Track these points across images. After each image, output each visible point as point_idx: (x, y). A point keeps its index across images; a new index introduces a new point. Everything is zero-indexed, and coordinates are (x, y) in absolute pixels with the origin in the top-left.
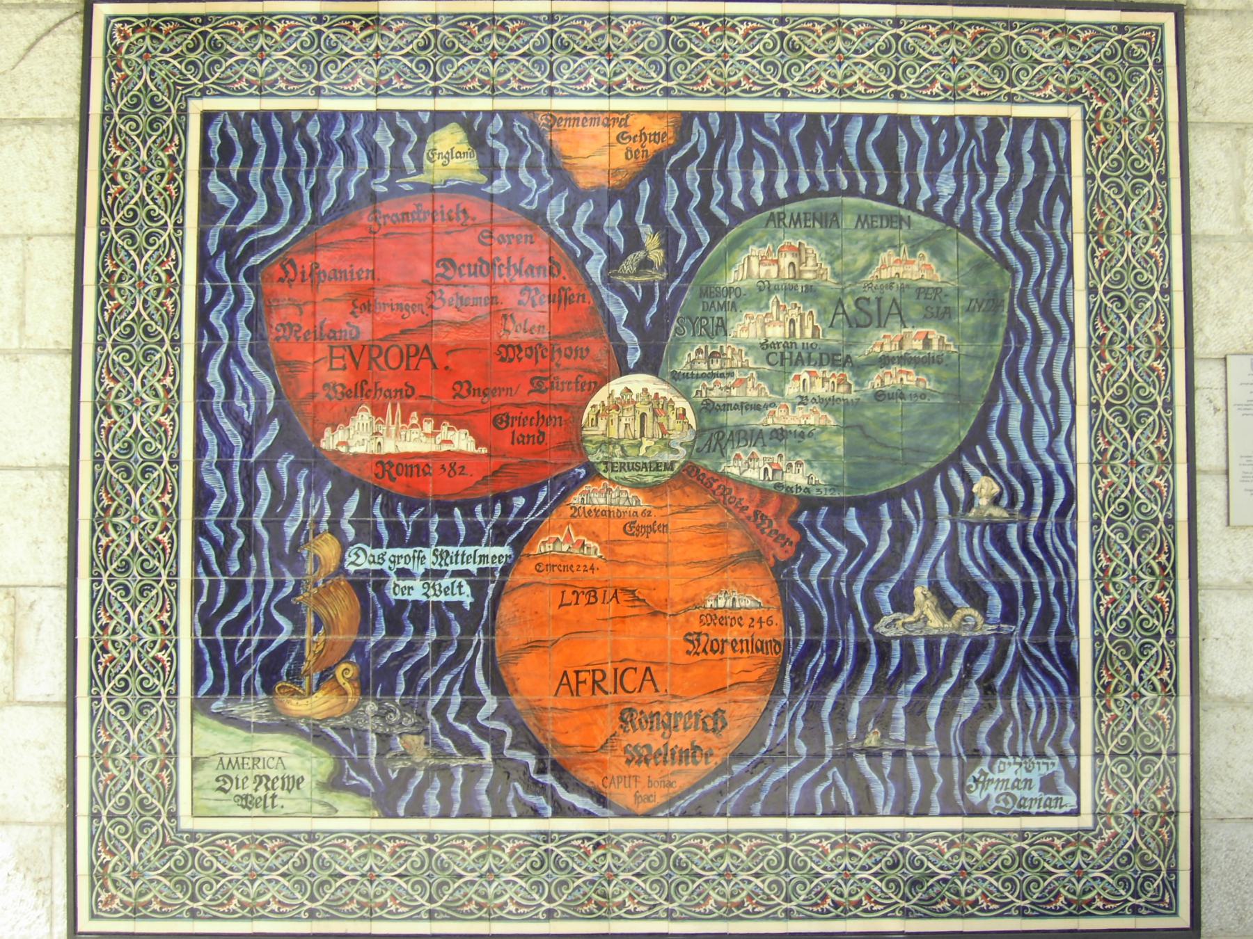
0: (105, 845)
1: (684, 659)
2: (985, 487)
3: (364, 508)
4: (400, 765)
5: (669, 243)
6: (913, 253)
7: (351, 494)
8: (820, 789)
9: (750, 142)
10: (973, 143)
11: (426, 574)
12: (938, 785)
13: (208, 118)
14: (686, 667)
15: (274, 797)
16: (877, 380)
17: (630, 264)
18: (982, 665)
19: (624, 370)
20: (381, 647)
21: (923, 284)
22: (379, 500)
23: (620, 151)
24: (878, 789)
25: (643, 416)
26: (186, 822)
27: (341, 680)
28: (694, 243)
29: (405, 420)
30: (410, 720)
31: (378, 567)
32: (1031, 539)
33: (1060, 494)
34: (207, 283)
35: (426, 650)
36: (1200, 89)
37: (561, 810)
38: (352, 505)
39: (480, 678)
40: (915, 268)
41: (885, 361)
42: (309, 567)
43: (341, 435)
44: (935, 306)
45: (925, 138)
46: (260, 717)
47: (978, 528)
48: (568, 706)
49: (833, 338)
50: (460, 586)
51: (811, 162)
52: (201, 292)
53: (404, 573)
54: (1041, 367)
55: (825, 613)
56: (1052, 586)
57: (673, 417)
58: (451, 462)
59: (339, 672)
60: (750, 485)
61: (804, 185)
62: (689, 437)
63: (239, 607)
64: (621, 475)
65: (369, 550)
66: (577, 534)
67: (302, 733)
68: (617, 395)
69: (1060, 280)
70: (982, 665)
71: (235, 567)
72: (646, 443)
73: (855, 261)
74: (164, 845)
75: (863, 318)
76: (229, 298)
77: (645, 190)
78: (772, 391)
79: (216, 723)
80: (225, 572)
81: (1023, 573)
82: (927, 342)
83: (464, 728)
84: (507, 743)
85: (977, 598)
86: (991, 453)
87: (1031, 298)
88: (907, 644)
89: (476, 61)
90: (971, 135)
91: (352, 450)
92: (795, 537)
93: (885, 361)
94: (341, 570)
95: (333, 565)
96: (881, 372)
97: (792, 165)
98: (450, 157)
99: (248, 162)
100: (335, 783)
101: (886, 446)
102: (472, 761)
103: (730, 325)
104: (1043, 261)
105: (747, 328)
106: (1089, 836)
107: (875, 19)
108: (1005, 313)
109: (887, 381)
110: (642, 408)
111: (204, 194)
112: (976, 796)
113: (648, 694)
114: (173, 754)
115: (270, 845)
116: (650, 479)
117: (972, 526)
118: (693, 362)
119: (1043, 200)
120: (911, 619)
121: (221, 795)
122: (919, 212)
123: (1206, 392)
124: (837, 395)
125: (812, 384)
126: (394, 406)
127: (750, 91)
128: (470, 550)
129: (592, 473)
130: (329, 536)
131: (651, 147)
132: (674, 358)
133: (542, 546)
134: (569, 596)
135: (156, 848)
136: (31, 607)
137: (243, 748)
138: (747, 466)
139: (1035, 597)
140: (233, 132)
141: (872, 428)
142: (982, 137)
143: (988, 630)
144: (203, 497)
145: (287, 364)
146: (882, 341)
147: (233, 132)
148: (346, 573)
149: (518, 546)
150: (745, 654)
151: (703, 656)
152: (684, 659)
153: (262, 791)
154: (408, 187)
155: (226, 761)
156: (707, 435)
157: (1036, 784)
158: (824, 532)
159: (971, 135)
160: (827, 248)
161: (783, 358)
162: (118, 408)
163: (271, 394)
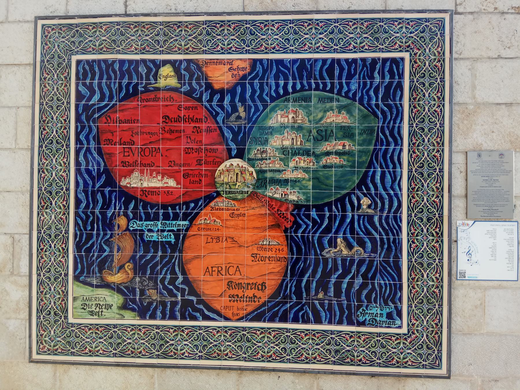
0: (42, 328)
1: (251, 263)
2: (365, 201)
3: (136, 207)
4: (147, 301)
5: (247, 109)
6: (340, 112)
7: (132, 202)
8: (301, 314)
9: (279, 71)
10: (365, 68)
11: (158, 231)
12: (346, 314)
13: (79, 62)
14: (252, 266)
15: (102, 312)
16: (324, 161)
17: (233, 117)
18: (363, 269)
19: (231, 157)
20: (142, 257)
21: (343, 124)
22: (141, 204)
23: (230, 74)
24: (323, 314)
25: (237, 174)
26: (71, 320)
27: (127, 269)
28: (257, 109)
29: (151, 175)
30: (151, 284)
31: (141, 228)
32: (383, 221)
33: (396, 204)
34: (79, 124)
35: (158, 258)
36: (459, 45)
37: (206, 318)
38: (132, 206)
39: (177, 269)
40: (340, 118)
41: (328, 154)
42: (116, 228)
43: (128, 180)
44: (347, 133)
45: (346, 67)
46: (98, 283)
47: (362, 217)
48: (208, 279)
49: (309, 145)
50: (170, 235)
51: (301, 78)
52: (77, 127)
53: (150, 231)
54: (389, 156)
55: (303, 247)
56: (392, 240)
57: (248, 174)
58: (167, 191)
59: (126, 266)
60: (276, 199)
61: (299, 86)
62: (254, 182)
63: (90, 243)
64: (229, 195)
65: (138, 222)
66: (213, 217)
67: (113, 289)
68: (228, 166)
69: (398, 121)
70: (363, 269)
71: (89, 228)
72: (238, 184)
73: (317, 116)
74: (63, 328)
75: (319, 138)
76: (87, 130)
77: (239, 90)
78: (285, 165)
79: (81, 285)
80: (86, 229)
81: (380, 235)
82: (344, 146)
83: (171, 287)
84: (186, 293)
85: (362, 243)
86: (368, 189)
87: (386, 129)
88: (335, 261)
89: (177, 40)
90: (365, 65)
91: (132, 186)
92: (293, 219)
93: (328, 154)
94: (127, 229)
95: (124, 227)
96: (326, 158)
97: (294, 78)
98: (167, 78)
99: (93, 78)
100: (124, 307)
101: (327, 186)
102: (173, 299)
103: (270, 140)
104: (391, 114)
105: (276, 142)
106: (406, 337)
107: (328, 20)
108: (375, 135)
109: (328, 161)
110: (237, 171)
111: (78, 92)
112: (361, 319)
113: (238, 276)
114: (66, 295)
115: (100, 329)
116: (239, 197)
117: (359, 216)
118: (256, 154)
119: (394, 90)
120: (336, 250)
121: (83, 311)
122: (343, 96)
123: (457, 165)
124: (309, 167)
125: (300, 163)
126: (147, 170)
127: (279, 51)
128: (174, 222)
129: (218, 194)
130: (123, 217)
131: (241, 73)
132: (249, 153)
133: (200, 221)
134: (210, 240)
135: (60, 329)
136: (19, 241)
137: (91, 293)
138: (275, 192)
139: (385, 244)
140: (87, 68)
141: (322, 178)
142: (368, 66)
143: (366, 255)
144: (78, 202)
145: (108, 154)
146: (326, 146)
147: (87, 68)
148: (129, 230)
149: (191, 221)
150: (273, 262)
151: (258, 262)
152: (251, 263)
153: (98, 309)
154: (151, 89)
155: (85, 298)
156: (260, 181)
157: (385, 315)
158: (303, 217)
159: (365, 65)
160: (307, 111)
161: (288, 153)
162: (47, 170)
163: (102, 164)
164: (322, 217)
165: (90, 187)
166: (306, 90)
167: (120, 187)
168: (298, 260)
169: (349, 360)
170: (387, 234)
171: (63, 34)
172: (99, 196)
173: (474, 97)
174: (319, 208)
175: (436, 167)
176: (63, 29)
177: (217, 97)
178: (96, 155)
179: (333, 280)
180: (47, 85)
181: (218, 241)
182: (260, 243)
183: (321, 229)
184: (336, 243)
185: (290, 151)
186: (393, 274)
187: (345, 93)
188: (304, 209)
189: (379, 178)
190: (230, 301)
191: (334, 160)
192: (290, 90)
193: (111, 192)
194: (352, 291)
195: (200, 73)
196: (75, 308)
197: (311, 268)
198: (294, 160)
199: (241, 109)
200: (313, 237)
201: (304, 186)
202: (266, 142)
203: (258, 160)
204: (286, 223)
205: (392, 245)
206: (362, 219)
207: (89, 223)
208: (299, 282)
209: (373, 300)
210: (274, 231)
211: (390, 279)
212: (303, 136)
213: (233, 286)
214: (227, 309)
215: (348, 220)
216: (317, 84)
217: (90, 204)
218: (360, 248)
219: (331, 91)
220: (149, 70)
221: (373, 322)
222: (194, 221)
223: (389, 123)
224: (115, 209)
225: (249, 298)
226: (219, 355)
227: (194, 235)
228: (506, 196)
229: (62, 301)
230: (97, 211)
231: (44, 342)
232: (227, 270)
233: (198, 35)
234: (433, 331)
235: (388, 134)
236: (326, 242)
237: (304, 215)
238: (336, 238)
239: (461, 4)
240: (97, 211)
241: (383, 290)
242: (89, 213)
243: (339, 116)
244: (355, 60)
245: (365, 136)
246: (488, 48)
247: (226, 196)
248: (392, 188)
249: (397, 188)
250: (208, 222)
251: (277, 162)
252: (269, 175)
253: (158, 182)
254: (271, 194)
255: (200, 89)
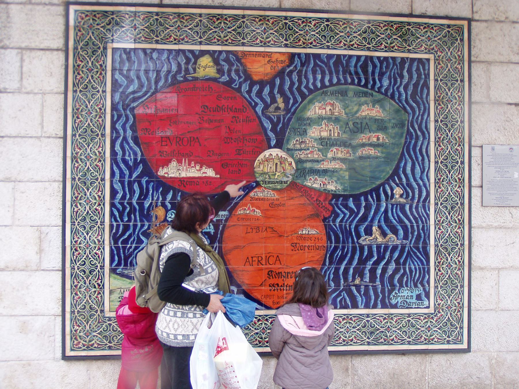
1: (290, 252)
2: (398, 191)
5: (286, 101)
7: (170, 192)
8: (339, 299)
10: (395, 67)
12: (380, 298)
14: (292, 256)
16: (360, 152)
17: (272, 108)
18: (396, 255)
19: (270, 147)
21: (377, 118)
22: (180, 194)
24: (359, 299)
25: (276, 164)
28: (295, 101)
29: (189, 165)
32: (414, 210)
33: (424, 194)
38: (170, 196)
41: (363, 145)
42: (154, 219)
43: (165, 170)
44: (380, 126)
45: (378, 65)
47: (395, 206)
51: (337, 73)
52: (112, 116)
54: (418, 148)
55: (341, 236)
61: (335, 80)
62: (293, 172)
64: (268, 185)
66: (252, 207)
69: (425, 117)
70: (396, 255)
71: (126, 219)
72: (278, 174)
73: (353, 109)
74: (99, 322)
75: (355, 130)
76: (123, 119)
77: (278, 81)
79: (119, 277)
80: (122, 221)
82: (378, 139)
85: (395, 232)
86: (400, 179)
87: (415, 124)
88: (370, 247)
89: (216, 32)
92: (331, 208)
93: (363, 145)
96: (361, 149)
97: (331, 73)
101: (363, 176)
103: (308, 131)
105: (314, 132)
109: (364, 152)
110: (276, 161)
112: (394, 302)
114: (102, 287)
116: (279, 187)
117: (393, 205)
118: (295, 144)
120: (372, 238)
125: (337, 153)
129: (258, 185)
132: (288, 143)
134: (249, 230)
138: (314, 183)
139: (415, 231)
140: (124, 56)
143: (399, 242)
144: (114, 192)
146: (362, 138)
150: (312, 251)
151: (297, 251)
152: (290, 252)
154: (190, 78)
156: (299, 171)
157: (415, 297)
158: (341, 207)
159: (394, 64)
160: (343, 104)
161: (326, 143)
163: (139, 154)
164: (358, 207)
165: (127, 177)
166: (342, 84)
167: (157, 177)
168: (336, 248)
169: (382, 340)
170: (417, 222)
171: (98, 21)
172: (136, 186)
173: (488, 97)
174: (356, 198)
175: (458, 159)
176: (97, 16)
177: (256, 88)
178: (132, 144)
179: (368, 267)
180: (81, 72)
181: (258, 231)
182: (300, 233)
183: (358, 218)
184: (371, 231)
185: (328, 142)
186: (422, 258)
187: (378, 88)
188: (341, 199)
189: (410, 169)
190: (270, 290)
191: (372, 152)
192: (327, 83)
193: (148, 183)
194: (386, 276)
195: (239, 64)
196: (113, 301)
197: (349, 255)
198: (332, 151)
199: (280, 100)
200: (350, 226)
201: (341, 176)
202: (305, 132)
203: (296, 150)
204: (324, 213)
205: (421, 231)
206: (395, 208)
207: (126, 214)
208: (337, 270)
209: (404, 283)
210: (312, 221)
211: (419, 263)
212: (340, 127)
213: (273, 276)
214: (268, 298)
215: (383, 209)
216: (353, 80)
217: (126, 194)
218: (393, 236)
219: (366, 86)
220: (188, 60)
221: (404, 304)
222: (234, 212)
223: (417, 118)
224: (153, 199)
225: (289, 286)
226: (260, 343)
227: (234, 225)
228: (514, 186)
229: (98, 295)
230: (134, 202)
231: (78, 337)
232: (267, 260)
233: (237, 27)
234: (455, 309)
235: (417, 128)
236: (363, 230)
237: (341, 204)
238: (371, 226)
239: (476, 12)
240: (134, 202)
241: (414, 274)
242: (125, 204)
243: (373, 110)
244: (386, 58)
245: (397, 129)
246: (500, 54)
247: (266, 186)
248: (421, 178)
249: (426, 178)
250: (248, 212)
251: (315, 153)
252: (308, 165)
253: (196, 172)
254: (310, 184)
255: (239, 79)
